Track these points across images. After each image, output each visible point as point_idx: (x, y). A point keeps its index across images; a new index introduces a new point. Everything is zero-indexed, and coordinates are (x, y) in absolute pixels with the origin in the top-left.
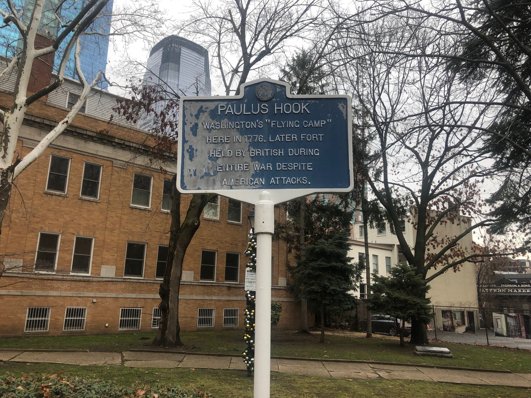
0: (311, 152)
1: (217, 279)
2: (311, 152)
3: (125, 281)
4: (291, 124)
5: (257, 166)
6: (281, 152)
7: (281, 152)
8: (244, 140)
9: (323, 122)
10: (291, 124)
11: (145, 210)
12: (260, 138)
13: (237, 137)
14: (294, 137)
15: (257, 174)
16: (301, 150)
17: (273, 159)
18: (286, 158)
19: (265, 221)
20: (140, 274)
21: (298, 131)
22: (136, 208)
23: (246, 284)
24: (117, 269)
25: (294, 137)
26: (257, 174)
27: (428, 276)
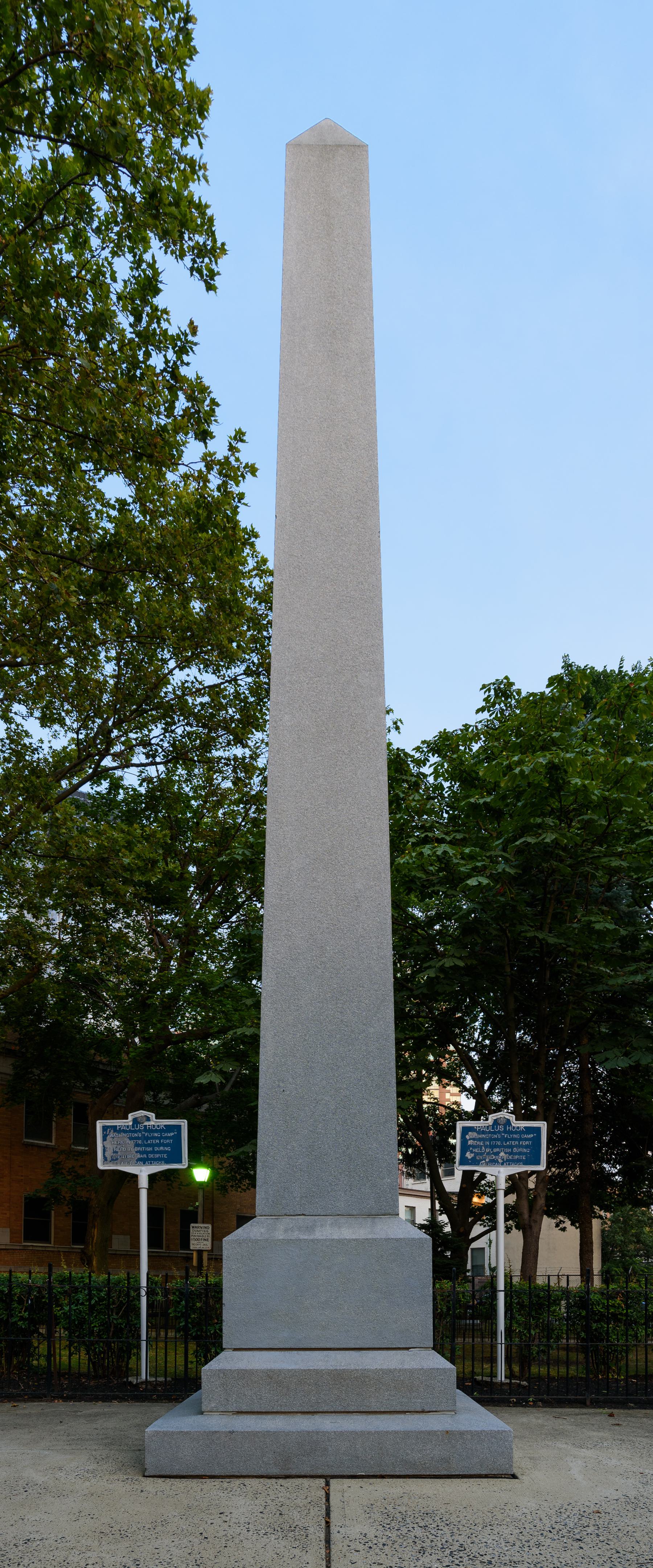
0: (166, 1149)
1: (168, 1247)
2: (166, 1149)
3: (25, 1248)
4: (156, 1135)
5: (139, 1156)
6: (151, 1149)
7: (151, 1149)
8: (131, 1143)
9: (172, 1134)
10: (156, 1135)
11: (47, 1147)
12: (140, 1142)
13: (128, 1141)
14: (158, 1141)
15: (139, 1160)
16: (161, 1148)
17: (147, 1153)
18: (153, 1152)
19: (144, 1182)
20: (48, 1240)
21: (160, 1138)
22: (32, 1145)
23: (192, 1242)
24: (12, 1233)
25: (158, 1141)
26: (139, 1160)
27: (473, 1235)
